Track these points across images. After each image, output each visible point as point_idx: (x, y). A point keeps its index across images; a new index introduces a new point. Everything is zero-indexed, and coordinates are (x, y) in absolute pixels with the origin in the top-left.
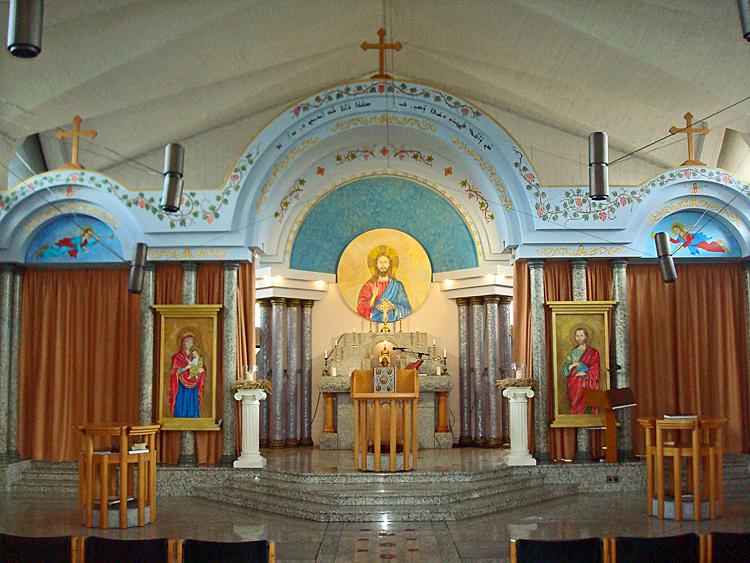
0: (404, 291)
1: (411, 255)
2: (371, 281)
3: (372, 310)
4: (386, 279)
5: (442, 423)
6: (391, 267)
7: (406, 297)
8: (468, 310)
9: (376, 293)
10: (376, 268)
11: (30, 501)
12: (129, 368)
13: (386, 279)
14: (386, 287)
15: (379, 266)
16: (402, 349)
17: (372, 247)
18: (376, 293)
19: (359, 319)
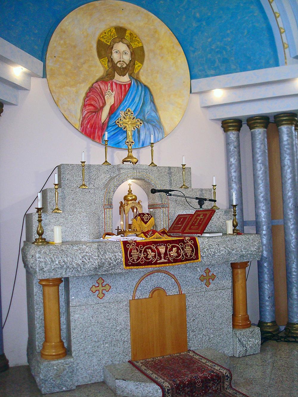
0: (153, 101)
1: (162, 48)
2: (102, 80)
3: (103, 127)
4: (125, 79)
5: (240, 314)
6: (132, 63)
7: (156, 110)
8: (238, 137)
9: (110, 99)
10: (111, 60)
11: (202, 363)
12: (97, 98)
13: (125, 79)
14: (126, 93)
15: (116, 57)
16: (167, 191)
17: (102, 27)
18: (110, 99)
19: (84, 141)
